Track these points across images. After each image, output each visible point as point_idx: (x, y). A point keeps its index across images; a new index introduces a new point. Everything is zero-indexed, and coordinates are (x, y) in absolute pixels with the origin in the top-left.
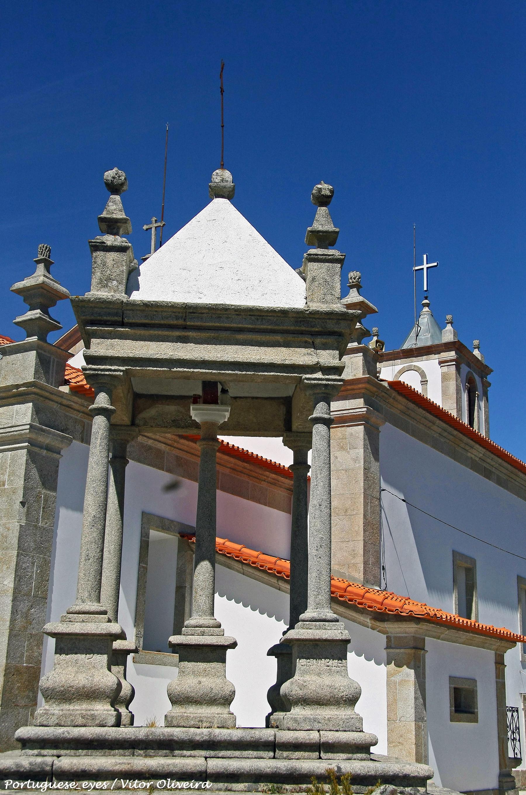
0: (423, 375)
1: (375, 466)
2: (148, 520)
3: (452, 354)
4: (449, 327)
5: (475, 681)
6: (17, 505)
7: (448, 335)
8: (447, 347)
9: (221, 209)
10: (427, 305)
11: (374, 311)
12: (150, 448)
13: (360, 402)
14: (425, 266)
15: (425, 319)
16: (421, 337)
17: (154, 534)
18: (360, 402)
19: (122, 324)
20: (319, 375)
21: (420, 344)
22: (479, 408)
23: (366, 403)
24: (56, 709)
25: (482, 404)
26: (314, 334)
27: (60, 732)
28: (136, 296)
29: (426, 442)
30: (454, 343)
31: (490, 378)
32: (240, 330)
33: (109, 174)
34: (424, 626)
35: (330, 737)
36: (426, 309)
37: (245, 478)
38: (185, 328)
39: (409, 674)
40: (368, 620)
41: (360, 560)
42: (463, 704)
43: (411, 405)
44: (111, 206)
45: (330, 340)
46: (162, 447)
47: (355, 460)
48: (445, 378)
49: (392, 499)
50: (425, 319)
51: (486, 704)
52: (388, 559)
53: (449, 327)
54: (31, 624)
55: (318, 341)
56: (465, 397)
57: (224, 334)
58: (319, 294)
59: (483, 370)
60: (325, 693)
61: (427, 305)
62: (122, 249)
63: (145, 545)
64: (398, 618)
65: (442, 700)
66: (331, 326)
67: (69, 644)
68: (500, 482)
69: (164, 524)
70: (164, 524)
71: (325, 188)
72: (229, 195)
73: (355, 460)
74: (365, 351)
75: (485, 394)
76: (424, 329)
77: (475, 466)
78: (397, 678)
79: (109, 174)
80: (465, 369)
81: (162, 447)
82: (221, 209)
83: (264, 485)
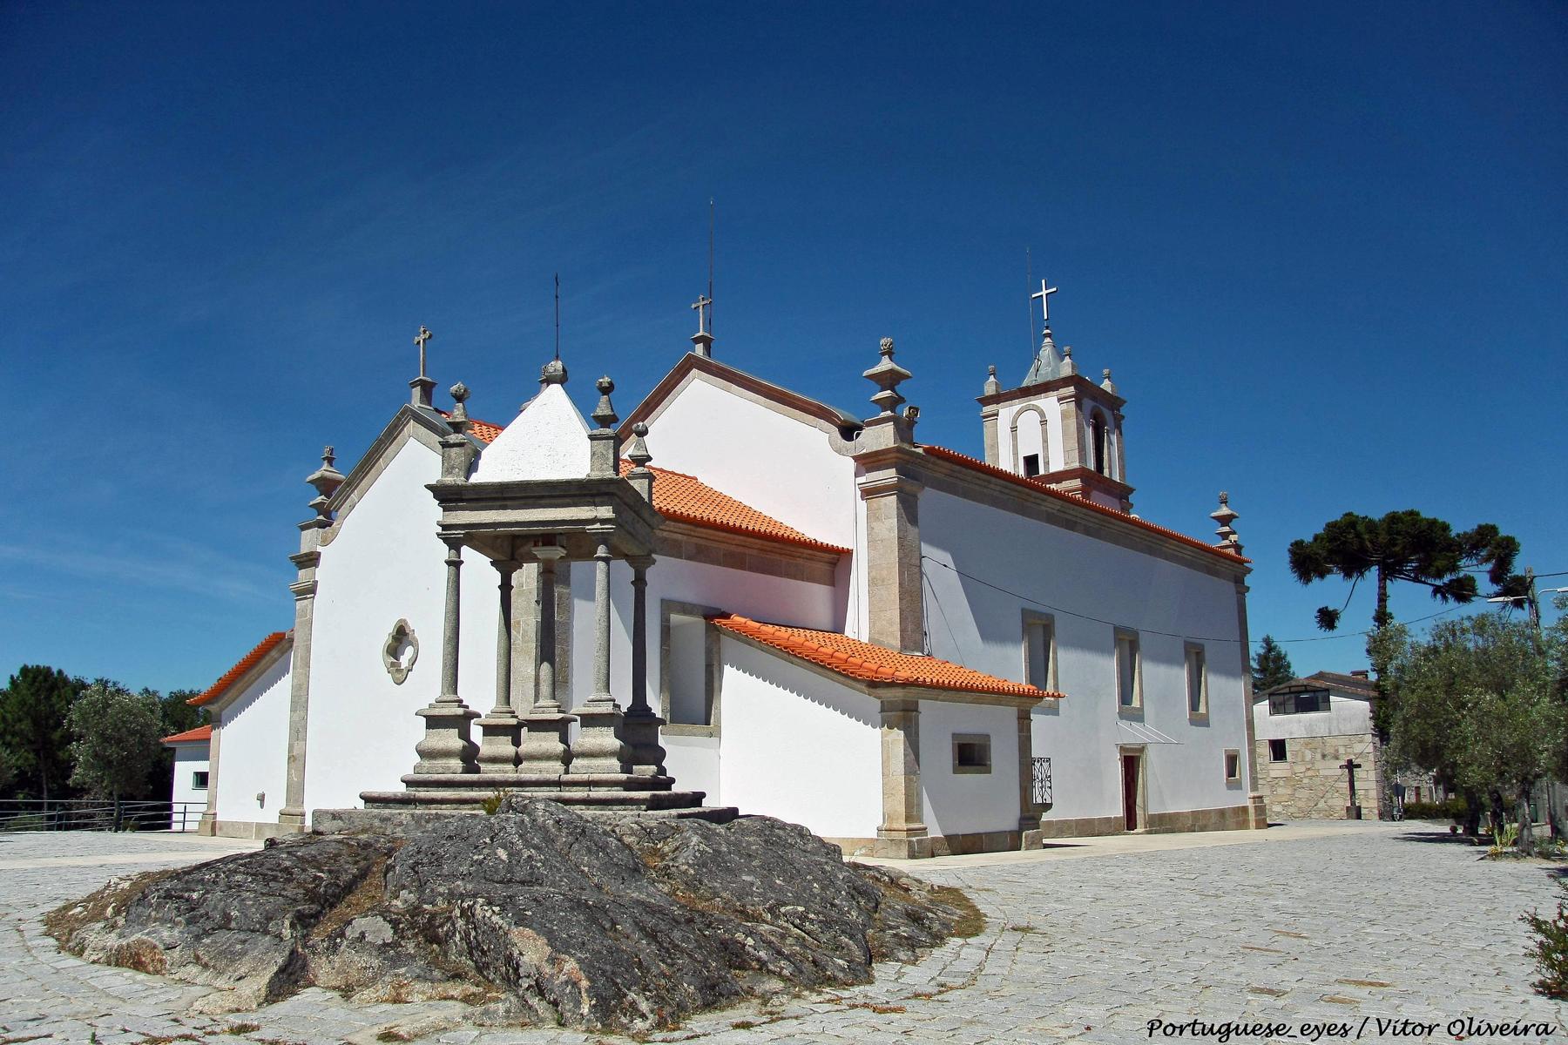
0: (1042, 414)
1: (913, 532)
2: (668, 606)
3: (1071, 390)
4: (1067, 360)
5: (988, 736)
6: (533, 604)
7: (1066, 368)
8: (1065, 382)
9: (554, 395)
10: (1049, 335)
11: (907, 377)
12: (666, 539)
13: (892, 472)
14: (1044, 292)
15: (1046, 352)
16: (1042, 371)
17: (675, 618)
18: (892, 472)
19: (462, 500)
20: (598, 526)
21: (1040, 380)
22: (1110, 443)
23: (898, 472)
24: (490, 767)
25: (1114, 438)
26: (593, 496)
27: (436, 777)
28: (475, 479)
29: (982, 502)
30: (1071, 378)
31: (1123, 411)
32: (542, 497)
33: (454, 388)
34: (914, 690)
35: (595, 777)
36: (1048, 340)
37: (778, 557)
38: (505, 499)
39: (898, 735)
40: (863, 687)
41: (897, 628)
42: (970, 755)
43: (957, 468)
44: (456, 412)
45: (606, 498)
46: (679, 537)
47: (890, 530)
48: (1064, 416)
49: (938, 564)
50: (1046, 352)
51: (1003, 756)
52: (932, 623)
53: (1067, 360)
54: (1541, 652)
55: (597, 500)
56: (1089, 432)
57: (530, 501)
58: (598, 465)
59: (1114, 402)
60: (596, 748)
61: (1049, 335)
62: (461, 445)
63: (666, 631)
64: (892, 685)
65: (940, 754)
66: (604, 489)
67: (589, 721)
68: (1088, 532)
69: (685, 608)
70: (685, 608)
71: (606, 380)
72: (562, 380)
73: (890, 530)
74: (896, 420)
75: (1119, 427)
76: (1049, 363)
77: (1051, 519)
78: (889, 738)
79: (454, 388)
80: (1088, 404)
81: (679, 537)
82: (554, 395)
83: (801, 561)
